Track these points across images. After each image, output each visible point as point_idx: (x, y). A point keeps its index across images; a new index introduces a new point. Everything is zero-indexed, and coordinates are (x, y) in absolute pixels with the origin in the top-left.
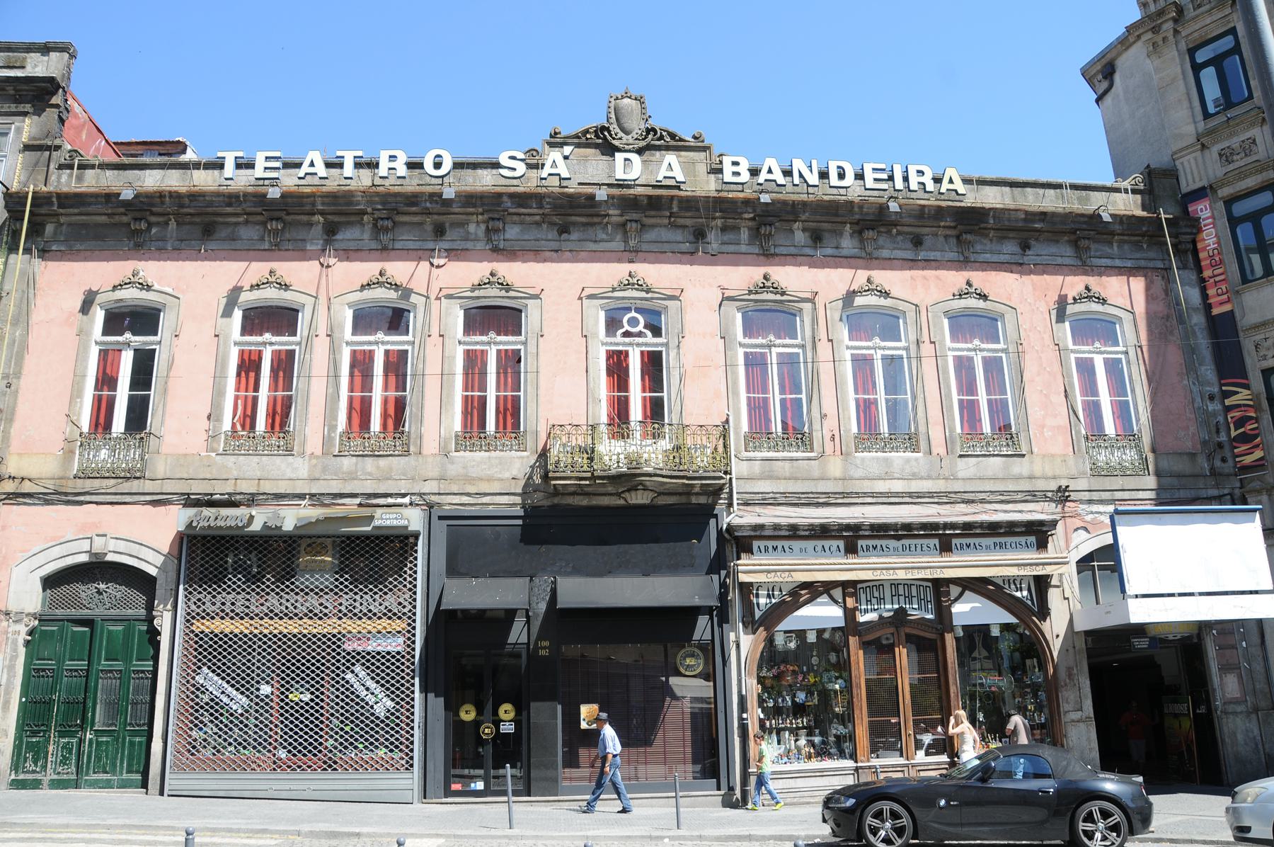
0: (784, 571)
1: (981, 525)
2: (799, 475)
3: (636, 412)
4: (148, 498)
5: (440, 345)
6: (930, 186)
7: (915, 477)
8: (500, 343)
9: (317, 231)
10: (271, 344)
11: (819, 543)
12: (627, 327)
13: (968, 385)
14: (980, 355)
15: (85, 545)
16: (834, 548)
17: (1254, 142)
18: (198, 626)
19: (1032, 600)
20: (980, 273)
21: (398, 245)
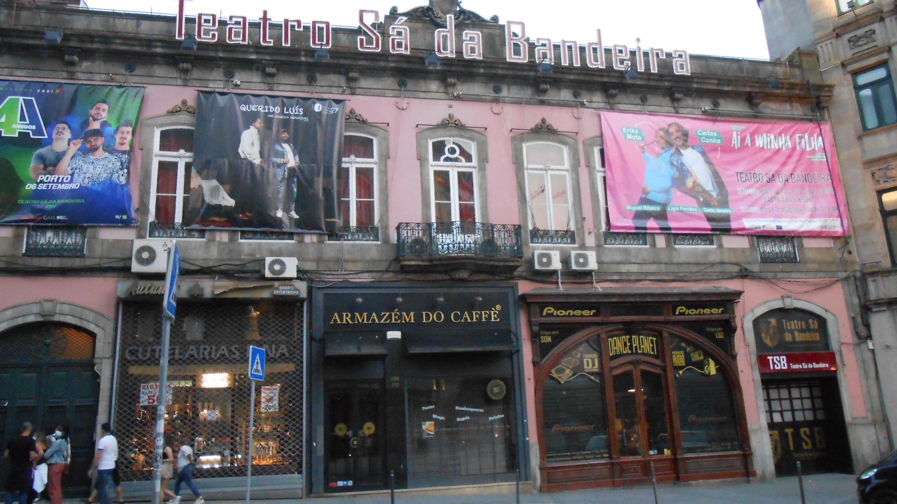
3: (455, 216)
8: (358, 163)
12: (447, 154)
15: (35, 309)
17: (874, 32)
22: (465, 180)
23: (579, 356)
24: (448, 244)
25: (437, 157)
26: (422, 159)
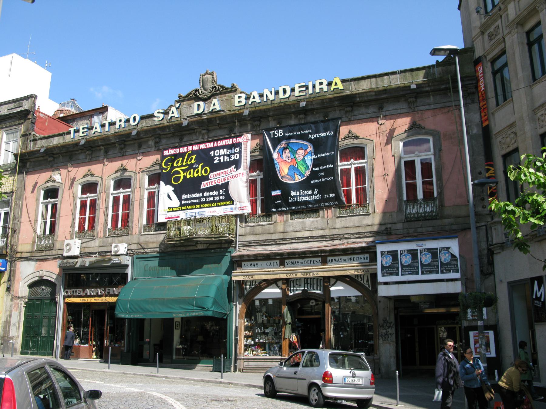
0: (250, 275)
1: (339, 250)
2: (265, 232)
4: (54, 257)
6: (325, 89)
7: (316, 229)
9: (102, 151)
10: (89, 197)
11: (269, 262)
14: (354, 166)
15: (37, 274)
16: (318, 261)
18: (68, 300)
19: (368, 285)
20: (356, 125)
21: (127, 153)
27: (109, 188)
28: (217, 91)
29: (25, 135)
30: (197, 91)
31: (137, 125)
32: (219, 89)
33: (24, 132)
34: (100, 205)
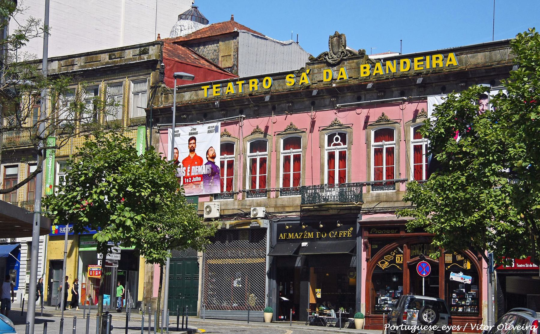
5: (277, 152)
13: (378, 162)
22: (343, 156)
23: (394, 254)
24: (334, 196)
25: (329, 145)
26: (321, 147)
27: (245, 151)
28: (345, 56)
29: (154, 88)
30: (326, 54)
31: (270, 88)
32: (347, 55)
33: (153, 84)
34: (237, 167)
